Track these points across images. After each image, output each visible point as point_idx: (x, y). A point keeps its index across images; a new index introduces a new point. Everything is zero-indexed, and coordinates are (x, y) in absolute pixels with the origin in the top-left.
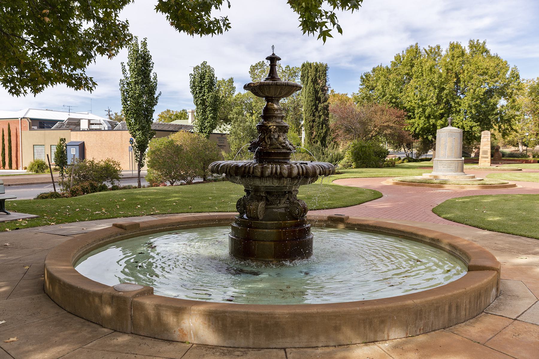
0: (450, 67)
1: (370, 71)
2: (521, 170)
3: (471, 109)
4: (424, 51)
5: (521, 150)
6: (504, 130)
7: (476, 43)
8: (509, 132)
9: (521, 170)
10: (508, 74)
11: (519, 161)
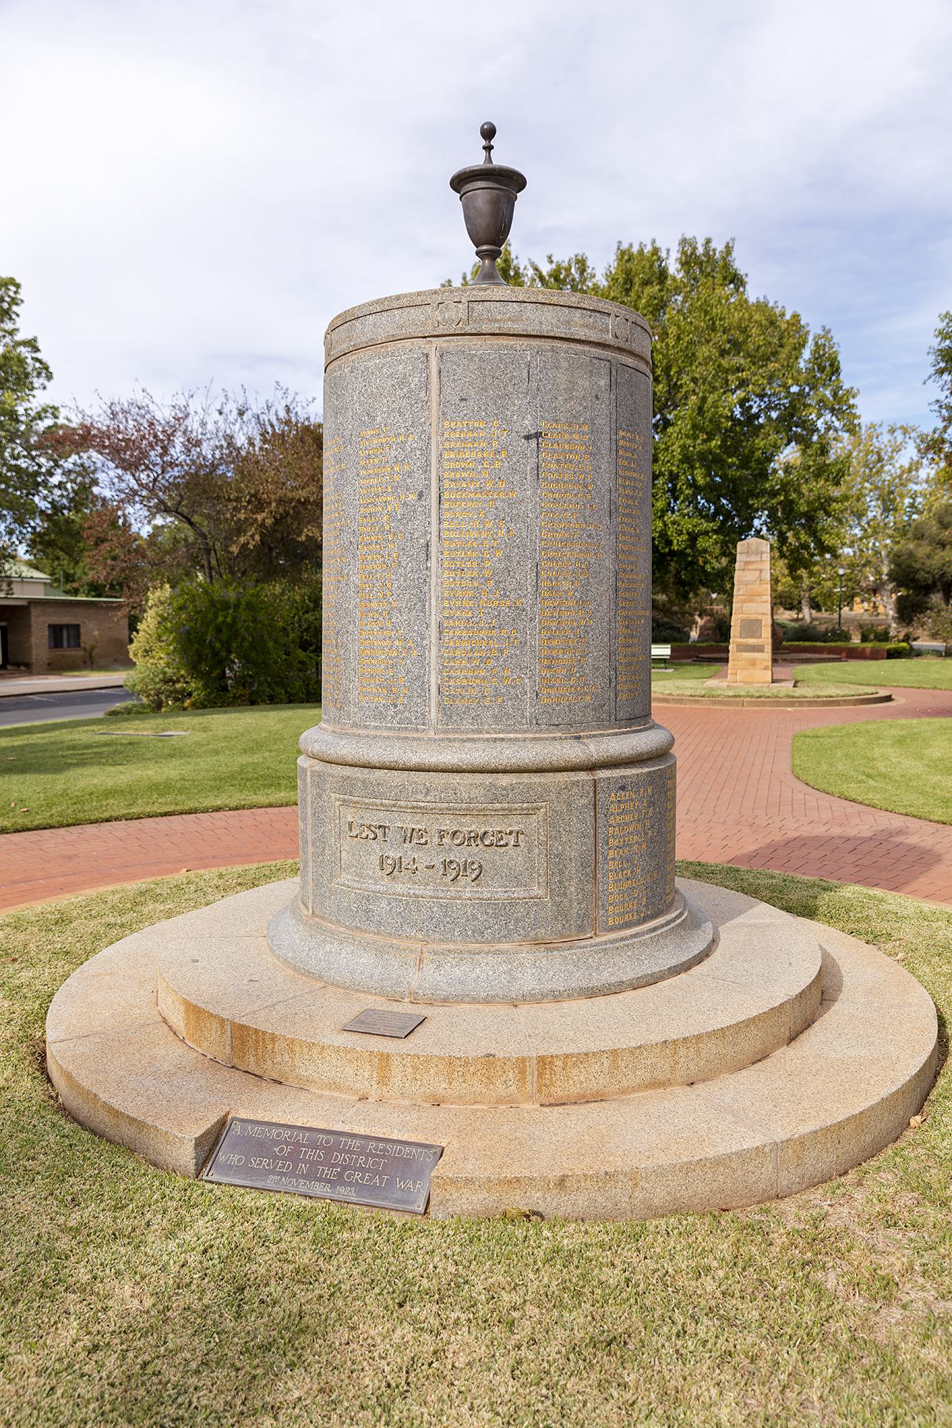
2: (888, 699)
3: (692, 467)
4: (530, 272)
5: (808, 618)
6: (797, 549)
7: (700, 250)
9: (888, 699)
11: (831, 651)
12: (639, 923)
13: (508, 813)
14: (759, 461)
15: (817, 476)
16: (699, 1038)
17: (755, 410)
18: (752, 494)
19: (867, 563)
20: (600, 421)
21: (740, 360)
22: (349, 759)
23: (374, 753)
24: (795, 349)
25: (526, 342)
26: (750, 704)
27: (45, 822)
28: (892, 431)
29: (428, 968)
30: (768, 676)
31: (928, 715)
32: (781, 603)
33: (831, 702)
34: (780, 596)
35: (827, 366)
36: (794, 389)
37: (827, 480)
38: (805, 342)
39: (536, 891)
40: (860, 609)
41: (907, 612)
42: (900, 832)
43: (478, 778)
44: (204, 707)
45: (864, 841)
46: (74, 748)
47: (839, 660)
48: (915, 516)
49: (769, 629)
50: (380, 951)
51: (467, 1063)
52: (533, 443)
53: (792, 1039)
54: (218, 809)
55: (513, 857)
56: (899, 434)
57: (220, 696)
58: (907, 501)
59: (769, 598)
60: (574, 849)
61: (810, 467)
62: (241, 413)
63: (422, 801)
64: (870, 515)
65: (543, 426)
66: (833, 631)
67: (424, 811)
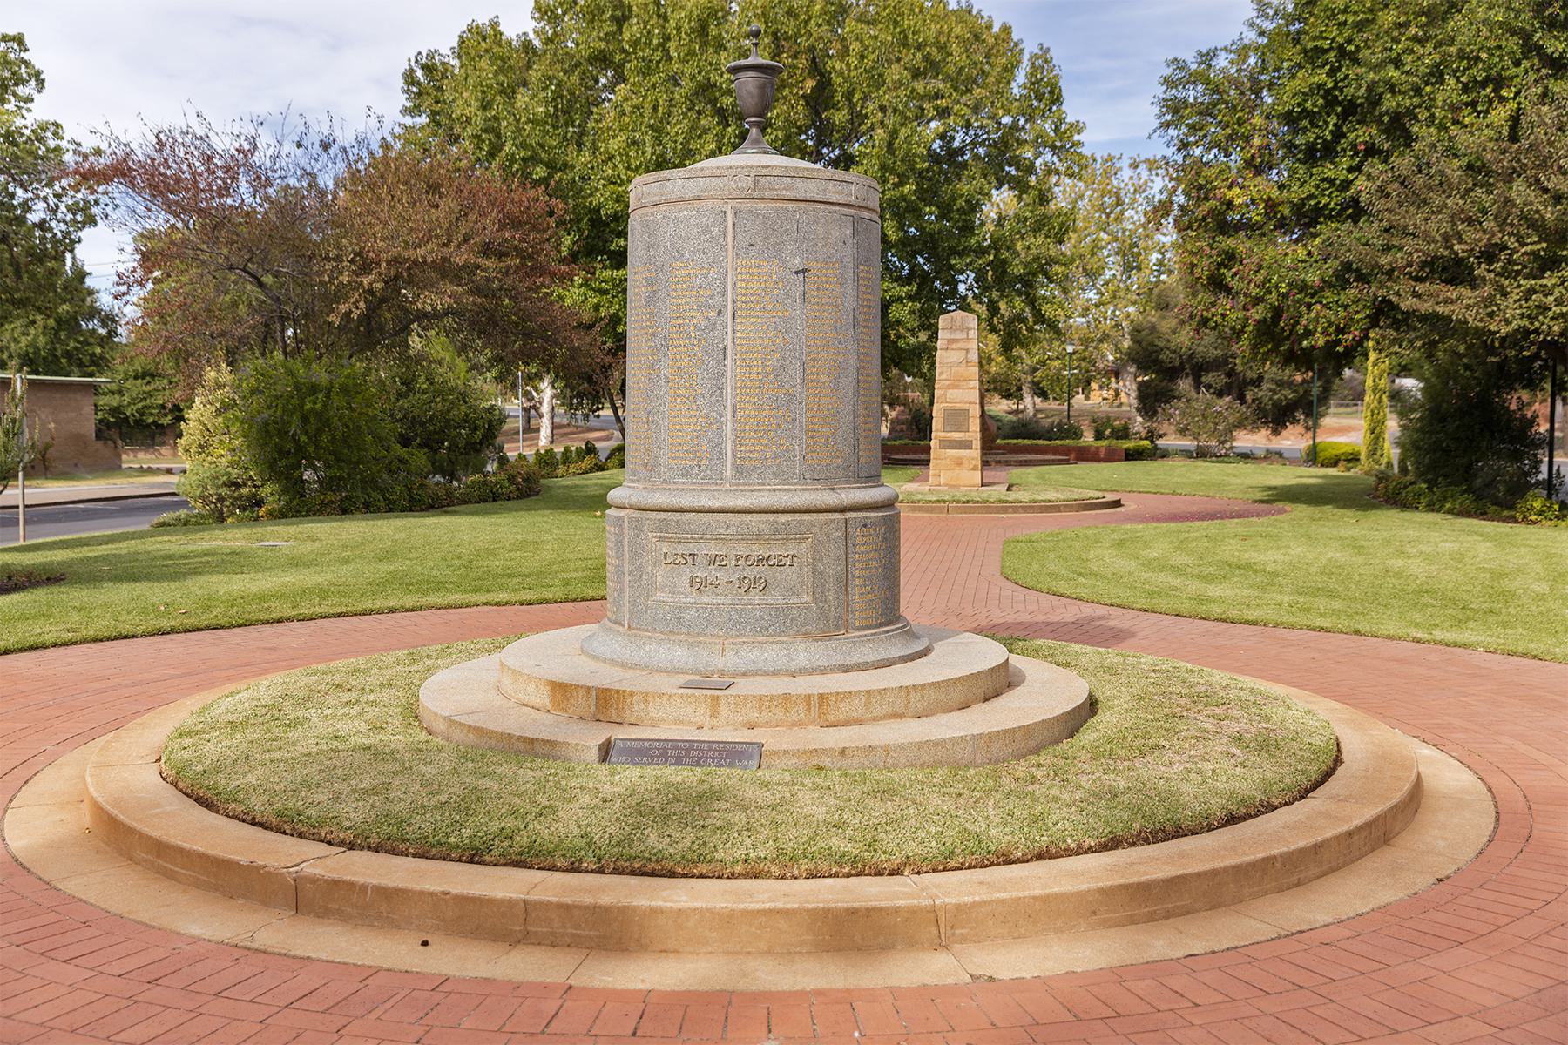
0: (789, 27)
1: (446, 51)
2: (1117, 504)
8: (1031, 330)
9: (1117, 504)
10: (1019, 83)
11: (1055, 450)
12: (880, 625)
13: (786, 541)
14: (961, 211)
15: (1036, 230)
16: (923, 686)
17: (957, 143)
18: (954, 252)
19: (1105, 338)
20: (847, 260)
21: (938, 84)
22: (665, 506)
23: (685, 501)
24: (1006, 70)
25: (795, 205)
26: (956, 510)
27: (214, 621)
28: (1134, 166)
29: (730, 654)
30: (976, 477)
31: (1158, 520)
32: (995, 390)
33: (1050, 507)
34: (994, 381)
35: (1047, 93)
36: (1007, 120)
37: (1047, 237)
38: (1019, 62)
39: (805, 598)
40: (1096, 400)
41: (1151, 400)
42: (1103, 618)
43: (764, 517)
44: (285, 516)
45: (1066, 624)
46: (169, 557)
47: (1067, 462)
48: (1163, 277)
49: (978, 421)
50: (691, 646)
51: (772, 699)
52: (801, 277)
53: (986, 700)
54: (393, 610)
55: (790, 574)
56: (1143, 169)
57: (298, 506)
58: (1155, 256)
59: (977, 384)
60: (832, 569)
61: (1026, 219)
62: (326, 146)
63: (724, 533)
64: (1108, 274)
65: (808, 265)
66: (1060, 425)
67: (725, 542)
